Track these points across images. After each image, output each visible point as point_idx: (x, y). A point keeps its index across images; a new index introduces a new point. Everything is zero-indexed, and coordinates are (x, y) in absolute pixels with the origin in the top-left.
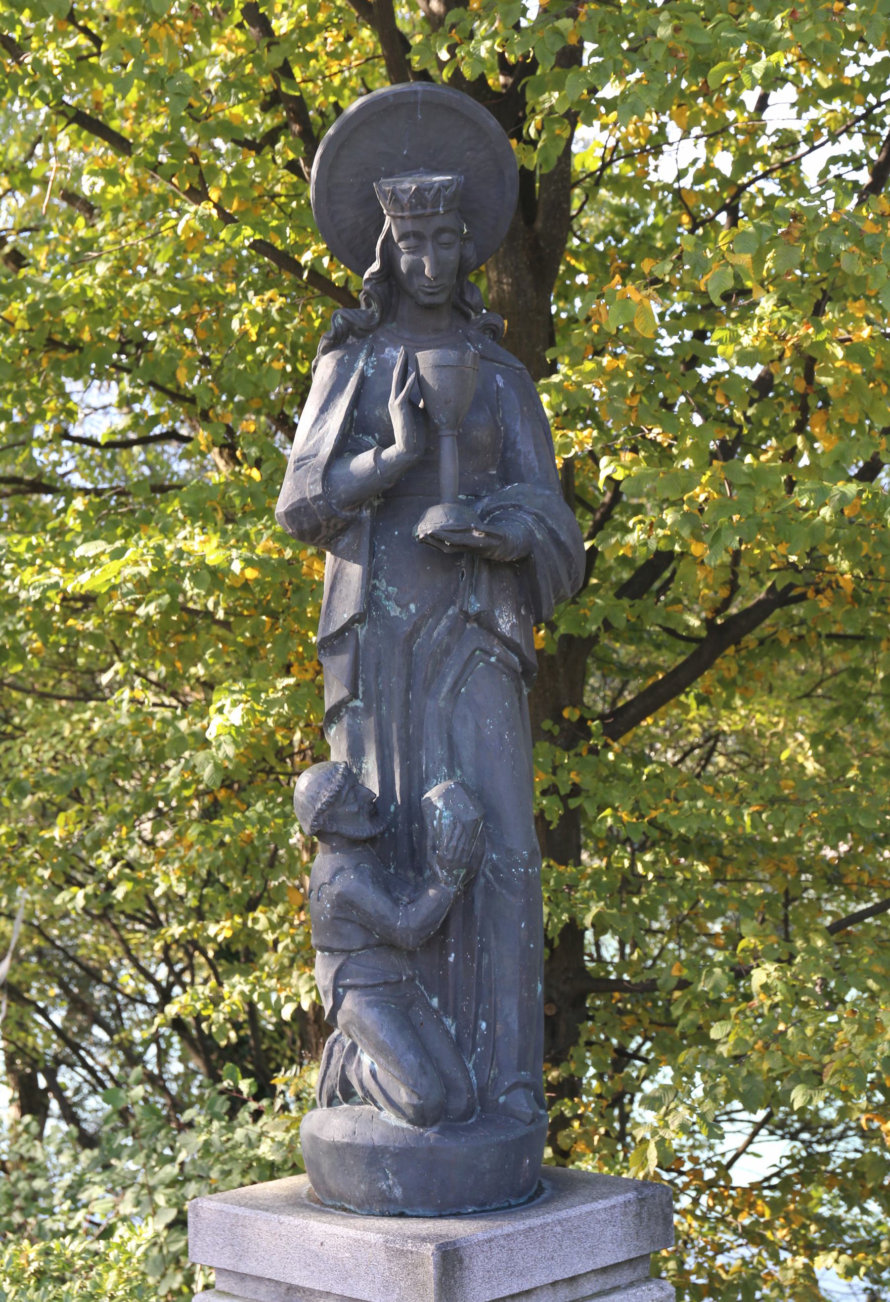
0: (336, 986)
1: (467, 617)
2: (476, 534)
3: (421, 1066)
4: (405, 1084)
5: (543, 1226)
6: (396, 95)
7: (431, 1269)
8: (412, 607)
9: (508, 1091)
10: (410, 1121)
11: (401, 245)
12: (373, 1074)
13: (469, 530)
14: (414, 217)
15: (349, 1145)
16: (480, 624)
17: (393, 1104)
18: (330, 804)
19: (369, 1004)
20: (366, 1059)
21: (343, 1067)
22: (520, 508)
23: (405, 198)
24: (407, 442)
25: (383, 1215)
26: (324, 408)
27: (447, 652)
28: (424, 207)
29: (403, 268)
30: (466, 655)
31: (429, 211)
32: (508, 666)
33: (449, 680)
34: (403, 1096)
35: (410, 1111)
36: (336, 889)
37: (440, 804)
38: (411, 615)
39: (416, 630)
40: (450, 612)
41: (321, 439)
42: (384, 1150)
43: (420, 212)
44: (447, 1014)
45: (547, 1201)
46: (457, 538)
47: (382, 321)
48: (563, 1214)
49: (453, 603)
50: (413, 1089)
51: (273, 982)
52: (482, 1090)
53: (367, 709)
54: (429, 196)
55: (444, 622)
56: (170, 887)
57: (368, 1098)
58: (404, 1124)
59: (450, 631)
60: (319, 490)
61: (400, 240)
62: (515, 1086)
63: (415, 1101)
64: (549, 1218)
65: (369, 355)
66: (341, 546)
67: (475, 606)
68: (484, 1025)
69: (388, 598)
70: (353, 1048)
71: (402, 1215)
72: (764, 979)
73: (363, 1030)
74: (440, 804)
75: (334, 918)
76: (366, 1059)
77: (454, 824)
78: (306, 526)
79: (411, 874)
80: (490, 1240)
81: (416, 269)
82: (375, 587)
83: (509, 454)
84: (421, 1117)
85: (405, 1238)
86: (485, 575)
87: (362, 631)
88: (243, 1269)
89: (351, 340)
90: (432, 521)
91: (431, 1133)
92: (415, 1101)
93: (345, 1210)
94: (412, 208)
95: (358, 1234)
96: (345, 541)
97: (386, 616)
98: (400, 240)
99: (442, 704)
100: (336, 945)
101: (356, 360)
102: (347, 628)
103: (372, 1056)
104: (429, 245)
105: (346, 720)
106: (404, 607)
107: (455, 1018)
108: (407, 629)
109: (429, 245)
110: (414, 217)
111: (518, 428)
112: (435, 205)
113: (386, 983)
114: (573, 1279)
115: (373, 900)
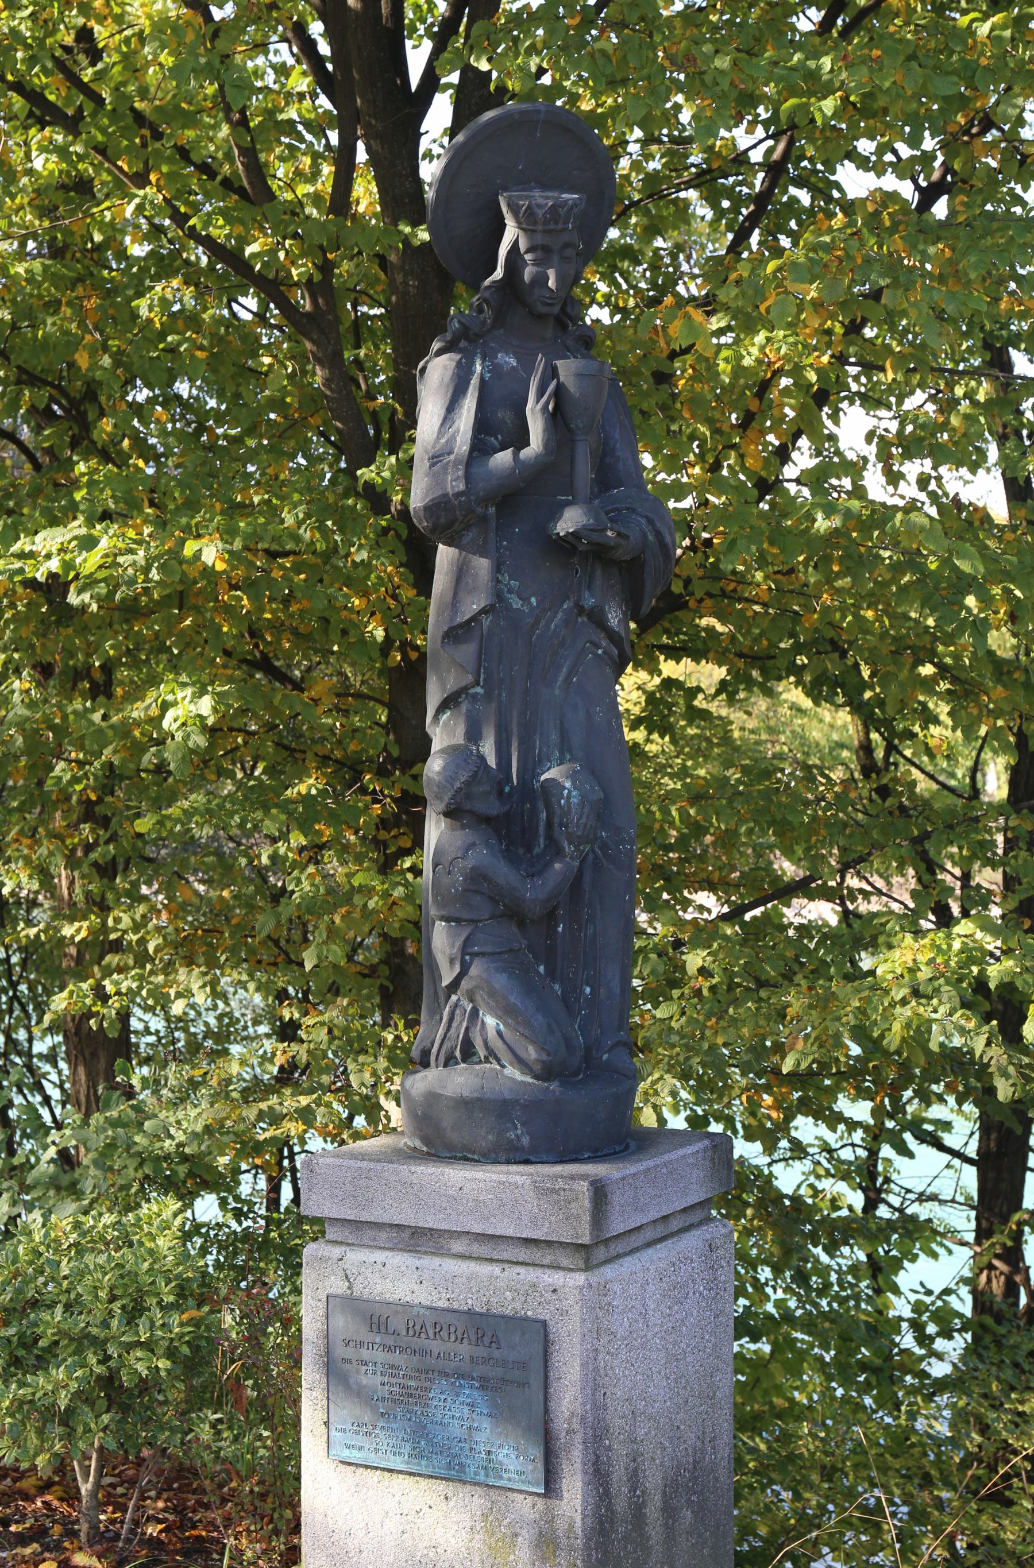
0: (464, 953)
1: (581, 610)
2: (609, 533)
3: (549, 1025)
4: (533, 1042)
5: (656, 1166)
6: (522, 113)
7: (587, 1203)
8: (533, 600)
9: (611, 1049)
10: (536, 1077)
11: (528, 257)
12: (499, 1033)
13: (605, 530)
14: (544, 231)
15: (478, 1099)
16: (590, 618)
17: (520, 1062)
18: (467, 783)
19: (497, 970)
20: (491, 1021)
21: (467, 1029)
22: (633, 510)
23: (540, 213)
24: (546, 444)
25: (508, 1162)
26: (452, 408)
28: (556, 223)
29: (527, 277)
31: (560, 226)
32: (610, 657)
34: (531, 1053)
35: (537, 1068)
36: (470, 863)
37: (568, 784)
38: (532, 608)
41: (453, 438)
42: (515, 1102)
43: (552, 227)
44: (554, 980)
45: (633, 1153)
46: (595, 537)
47: (494, 326)
48: (666, 1157)
49: (568, 598)
50: (541, 1048)
51: (161, 978)
52: (588, 1049)
53: (488, 696)
54: (562, 212)
55: (560, 615)
56: (19, 885)
57: (492, 1054)
58: (529, 1079)
60: (462, 487)
61: (527, 252)
62: (617, 1044)
63: (545, 1057)
64: (658, 1161)
65: (484, 361)
66: (465, 540)
67: (590, 602)
68: (588, 990)
69: (510, 591)
70: (475, 1012)
71: (527, 1162)
72: (700, 963)
73: (492, 993)
74: (568, 784)
75: (465, 890)
76: (491, 1021)
77: (582, 804)
78: (442, 520)
79: (521, 851)
80: (623, 1179)
81: (541, 280)
82: (498, 581)
83: (608, 460)
84: (546, 1073)
85: (556, 1177)
86: (599, 573)
87: (486, 621)
88: (366, 1217)
89: (463, 344)
90: (570, 521)
91: (554, 1086)
92: (545, 1057)
93: (467, 1159)
94: (546, 222)
95: (503, 1178)
96: (469, 537)
97: (508, 608)
98: (527, 252)
99: (557, 692)
100: (465, 915)
101: (472, 363)
102: (474, 618)
103: (498, 1017)
104: (556, 258)
105: (464, 707)
106: (525, 600)
107: (562, 984)
108: (530, 620)
109: (556, 258)
110: (544, 231)
111: (617, 436)
112: (566, 222)
113: (511, 951)
114: (665, 1218)
115: (504, 873)
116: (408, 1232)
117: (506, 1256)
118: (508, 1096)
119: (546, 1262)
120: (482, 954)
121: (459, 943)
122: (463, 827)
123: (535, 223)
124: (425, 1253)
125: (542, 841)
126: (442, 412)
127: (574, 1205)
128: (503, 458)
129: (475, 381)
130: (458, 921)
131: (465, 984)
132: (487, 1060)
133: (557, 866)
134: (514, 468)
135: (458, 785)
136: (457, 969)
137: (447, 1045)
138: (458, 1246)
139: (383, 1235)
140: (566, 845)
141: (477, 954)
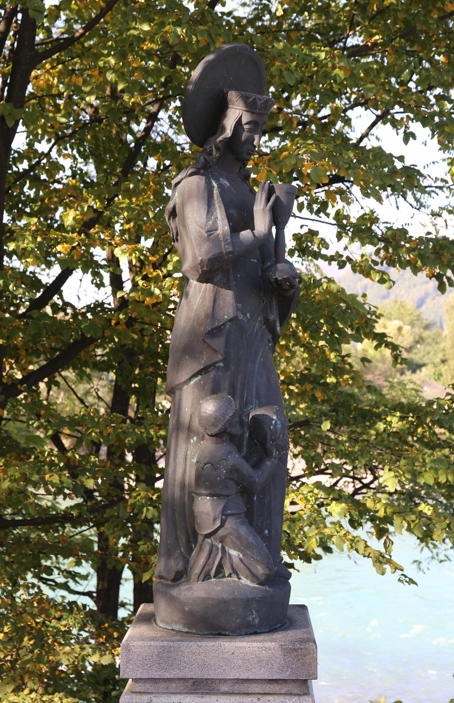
8: (248, 315)
10: (259, 584)
11: (246, 127)
15: (233, 599)
17: (254, 577)
20: (233, 553)
29: (243, 138)
37: (275, 417)
42: (253, 599)
53: (226, 368)
55: (257, 324)
57: (235, 572)
66: (216, 280)
71: (255, 633)
73: (239, 537)
74: (275, 417)
75: (226, 478)
76: (233, 553)
96: (218, 278)
103: (240, 551)
105: (212, 374)
115: (246, 468)
116: (190, 682)
117: (257, 690)
118: (225, 596)
119: (283, 691)
120: (232, 515)
121: (220, 508)
122: (223, 442)
123: (255, 108)
124: (203, 693)
125: (245, 449)
126: (206, 207)
127: (307, 657)
128: (246, 234)
129: (216, 192)
130: (218, 496)
131: (221, 533)
132: (230, 576)
133: (268, 463)
134: (254, 241)
135: (228, 418)
136: (218, 524)
137: (207, 568)
138: (224, 688)
139: (174, 685)
140: (274, 451)
141: (229, 515)
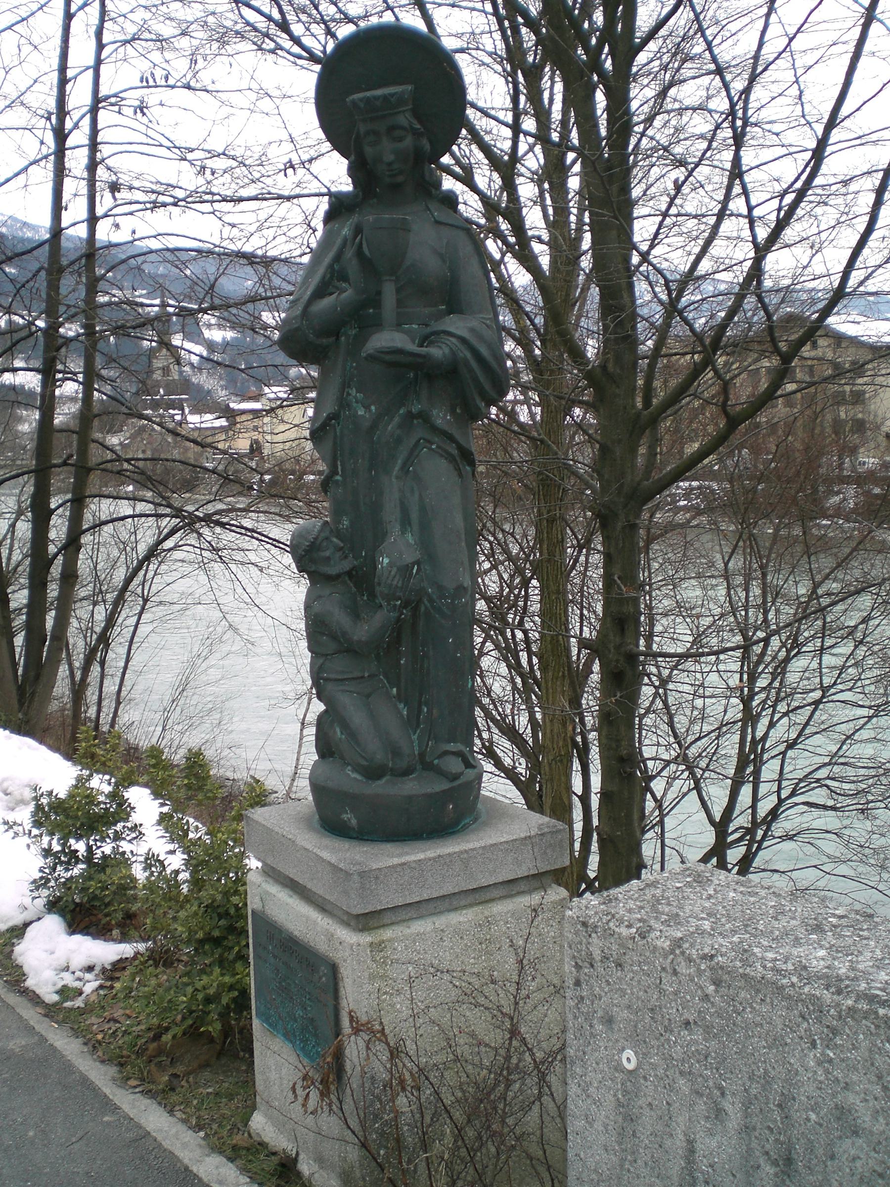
8: (373, 408)
27: (399, 441)
30: (413, 441)
33: (400, 462)
39: (373, 427)
40: (401, 412)
49: (404, 405)
59: (400, 426)
106: (367, 408)
115: (340, 618)
